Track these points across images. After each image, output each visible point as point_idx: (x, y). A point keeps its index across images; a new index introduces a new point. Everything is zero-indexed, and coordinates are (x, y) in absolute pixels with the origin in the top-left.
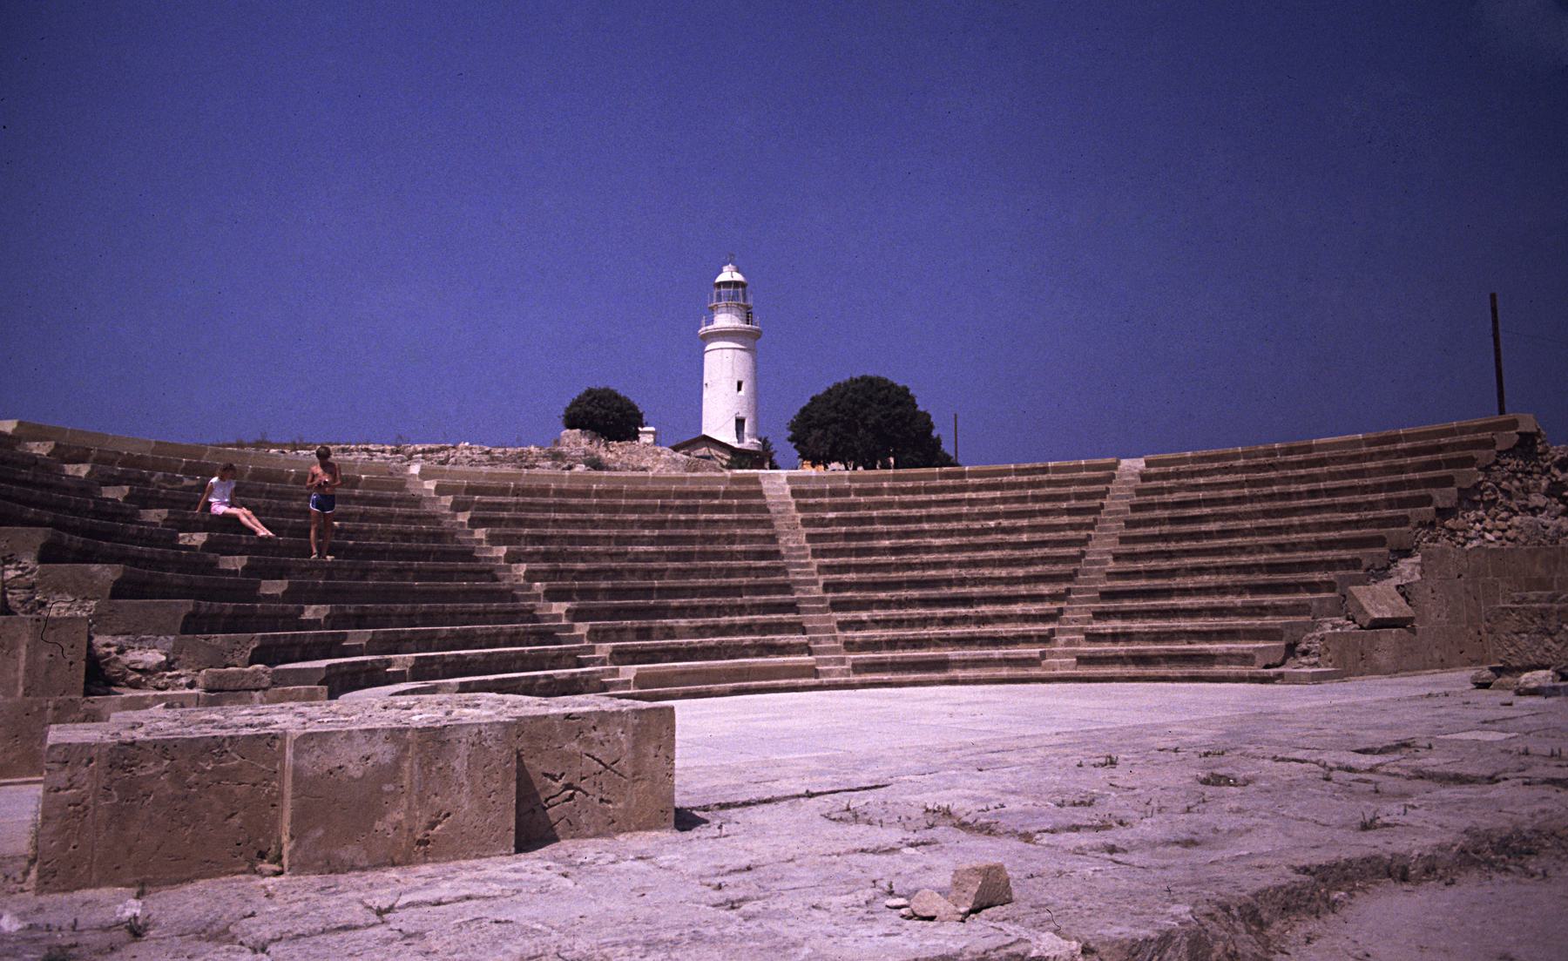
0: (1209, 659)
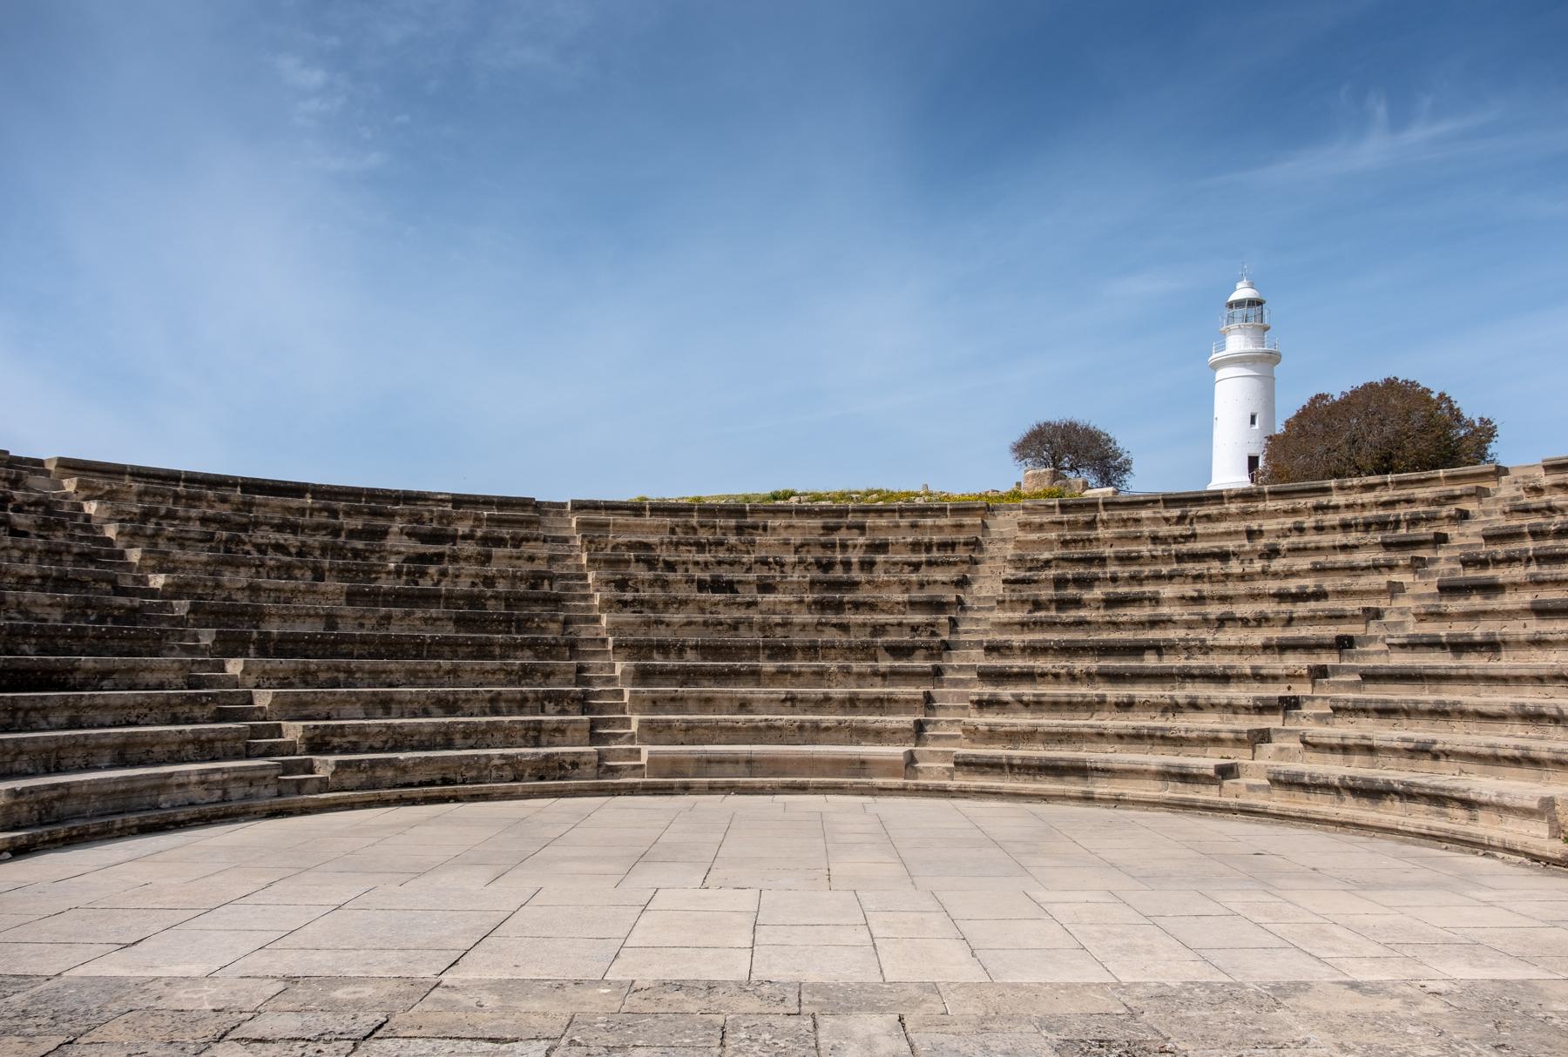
0: (1080, 770)
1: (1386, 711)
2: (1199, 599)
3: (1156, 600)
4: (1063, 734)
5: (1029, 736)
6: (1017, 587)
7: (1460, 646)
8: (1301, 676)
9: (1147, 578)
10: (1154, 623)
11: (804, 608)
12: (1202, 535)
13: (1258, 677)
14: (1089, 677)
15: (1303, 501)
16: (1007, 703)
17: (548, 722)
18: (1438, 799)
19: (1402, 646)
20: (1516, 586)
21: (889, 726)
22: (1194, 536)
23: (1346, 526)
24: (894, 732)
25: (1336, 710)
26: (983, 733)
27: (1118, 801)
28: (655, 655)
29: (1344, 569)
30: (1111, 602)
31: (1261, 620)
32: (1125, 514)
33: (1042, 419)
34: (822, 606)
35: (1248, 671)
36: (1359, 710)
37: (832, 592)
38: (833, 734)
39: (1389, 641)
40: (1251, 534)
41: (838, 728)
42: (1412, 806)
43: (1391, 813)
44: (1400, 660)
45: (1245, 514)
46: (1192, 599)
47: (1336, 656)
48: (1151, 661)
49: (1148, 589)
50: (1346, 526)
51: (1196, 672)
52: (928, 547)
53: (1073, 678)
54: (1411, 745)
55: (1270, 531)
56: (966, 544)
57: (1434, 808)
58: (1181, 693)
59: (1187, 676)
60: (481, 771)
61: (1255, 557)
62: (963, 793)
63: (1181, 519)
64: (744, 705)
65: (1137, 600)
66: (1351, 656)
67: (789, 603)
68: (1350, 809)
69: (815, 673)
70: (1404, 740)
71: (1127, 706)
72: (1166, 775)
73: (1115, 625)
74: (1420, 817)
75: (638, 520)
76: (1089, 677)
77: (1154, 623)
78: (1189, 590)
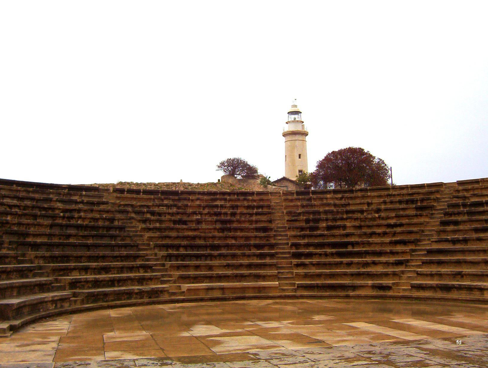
1: (440, 263)
2: (360, 227)
3: (344, 227)
4: (331, 275)
5: (319, 276)
6: (292, 222)
7: (454, 242)
8: (407, 252)
9: (339, 219)
10: (347, 235)
11: (216, 231)
12: (352, 204)
13: (392, 253)
14: (332, 254)
15: (383, 193)
16: (307, 265)
17: (147, 276)
18: (470, 289)
19: (436, 242)
20: (465, 222)
21: (268, 274)
22: (349, 204)
23: (400, 202)
24: (270, 276)
25: (423, 263)
26: (303, 275)
27: (359, 297)
28: (169, 250)
29: (406, 216)
30: (329, 228)
31: (385, 234)
32: (322, 196)
33: (236, 156)
34: (222, 230)
35: (389, 251)
36: (431, 263)
37: (225, 226)
38: (247, 278)
39: (432, 240)
40: (369, 204)
41: (250, 275)
42: (460, 292)
43: (454, 295)
44: (435, 247)
45: (363, 197)
46: (358, 226)
47: (414, 246)
48: (350, 249)
49: (339, 223)
50: (400, 202)
51: (370, 252)
52: (253, 207)
53: (326, 255)
54: (454, 273)
55: (375, 203)
56: (226, 207)
57: (469, 292)
58: (369, 259)
59: (367, 253)
60: (129, 294)
61: (373, 212)
62: (302, 297)
63: (341, 198)
64: (210, 268)
65: (338, 227)
66: (419, 245)
67: (211, 229)
68: (439, 294)
69: (232, 256)
70: (451, 271)
71: (349, 264)
72: (374, 287)
73: (334, 236)
74: (464, 295)
75: (139, 196)
76: (332, 254)
77: (347, 235)
78: (357, 223)
